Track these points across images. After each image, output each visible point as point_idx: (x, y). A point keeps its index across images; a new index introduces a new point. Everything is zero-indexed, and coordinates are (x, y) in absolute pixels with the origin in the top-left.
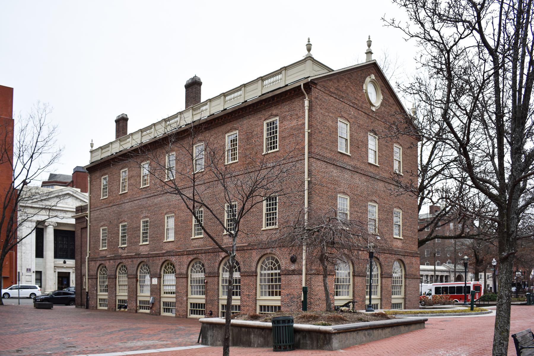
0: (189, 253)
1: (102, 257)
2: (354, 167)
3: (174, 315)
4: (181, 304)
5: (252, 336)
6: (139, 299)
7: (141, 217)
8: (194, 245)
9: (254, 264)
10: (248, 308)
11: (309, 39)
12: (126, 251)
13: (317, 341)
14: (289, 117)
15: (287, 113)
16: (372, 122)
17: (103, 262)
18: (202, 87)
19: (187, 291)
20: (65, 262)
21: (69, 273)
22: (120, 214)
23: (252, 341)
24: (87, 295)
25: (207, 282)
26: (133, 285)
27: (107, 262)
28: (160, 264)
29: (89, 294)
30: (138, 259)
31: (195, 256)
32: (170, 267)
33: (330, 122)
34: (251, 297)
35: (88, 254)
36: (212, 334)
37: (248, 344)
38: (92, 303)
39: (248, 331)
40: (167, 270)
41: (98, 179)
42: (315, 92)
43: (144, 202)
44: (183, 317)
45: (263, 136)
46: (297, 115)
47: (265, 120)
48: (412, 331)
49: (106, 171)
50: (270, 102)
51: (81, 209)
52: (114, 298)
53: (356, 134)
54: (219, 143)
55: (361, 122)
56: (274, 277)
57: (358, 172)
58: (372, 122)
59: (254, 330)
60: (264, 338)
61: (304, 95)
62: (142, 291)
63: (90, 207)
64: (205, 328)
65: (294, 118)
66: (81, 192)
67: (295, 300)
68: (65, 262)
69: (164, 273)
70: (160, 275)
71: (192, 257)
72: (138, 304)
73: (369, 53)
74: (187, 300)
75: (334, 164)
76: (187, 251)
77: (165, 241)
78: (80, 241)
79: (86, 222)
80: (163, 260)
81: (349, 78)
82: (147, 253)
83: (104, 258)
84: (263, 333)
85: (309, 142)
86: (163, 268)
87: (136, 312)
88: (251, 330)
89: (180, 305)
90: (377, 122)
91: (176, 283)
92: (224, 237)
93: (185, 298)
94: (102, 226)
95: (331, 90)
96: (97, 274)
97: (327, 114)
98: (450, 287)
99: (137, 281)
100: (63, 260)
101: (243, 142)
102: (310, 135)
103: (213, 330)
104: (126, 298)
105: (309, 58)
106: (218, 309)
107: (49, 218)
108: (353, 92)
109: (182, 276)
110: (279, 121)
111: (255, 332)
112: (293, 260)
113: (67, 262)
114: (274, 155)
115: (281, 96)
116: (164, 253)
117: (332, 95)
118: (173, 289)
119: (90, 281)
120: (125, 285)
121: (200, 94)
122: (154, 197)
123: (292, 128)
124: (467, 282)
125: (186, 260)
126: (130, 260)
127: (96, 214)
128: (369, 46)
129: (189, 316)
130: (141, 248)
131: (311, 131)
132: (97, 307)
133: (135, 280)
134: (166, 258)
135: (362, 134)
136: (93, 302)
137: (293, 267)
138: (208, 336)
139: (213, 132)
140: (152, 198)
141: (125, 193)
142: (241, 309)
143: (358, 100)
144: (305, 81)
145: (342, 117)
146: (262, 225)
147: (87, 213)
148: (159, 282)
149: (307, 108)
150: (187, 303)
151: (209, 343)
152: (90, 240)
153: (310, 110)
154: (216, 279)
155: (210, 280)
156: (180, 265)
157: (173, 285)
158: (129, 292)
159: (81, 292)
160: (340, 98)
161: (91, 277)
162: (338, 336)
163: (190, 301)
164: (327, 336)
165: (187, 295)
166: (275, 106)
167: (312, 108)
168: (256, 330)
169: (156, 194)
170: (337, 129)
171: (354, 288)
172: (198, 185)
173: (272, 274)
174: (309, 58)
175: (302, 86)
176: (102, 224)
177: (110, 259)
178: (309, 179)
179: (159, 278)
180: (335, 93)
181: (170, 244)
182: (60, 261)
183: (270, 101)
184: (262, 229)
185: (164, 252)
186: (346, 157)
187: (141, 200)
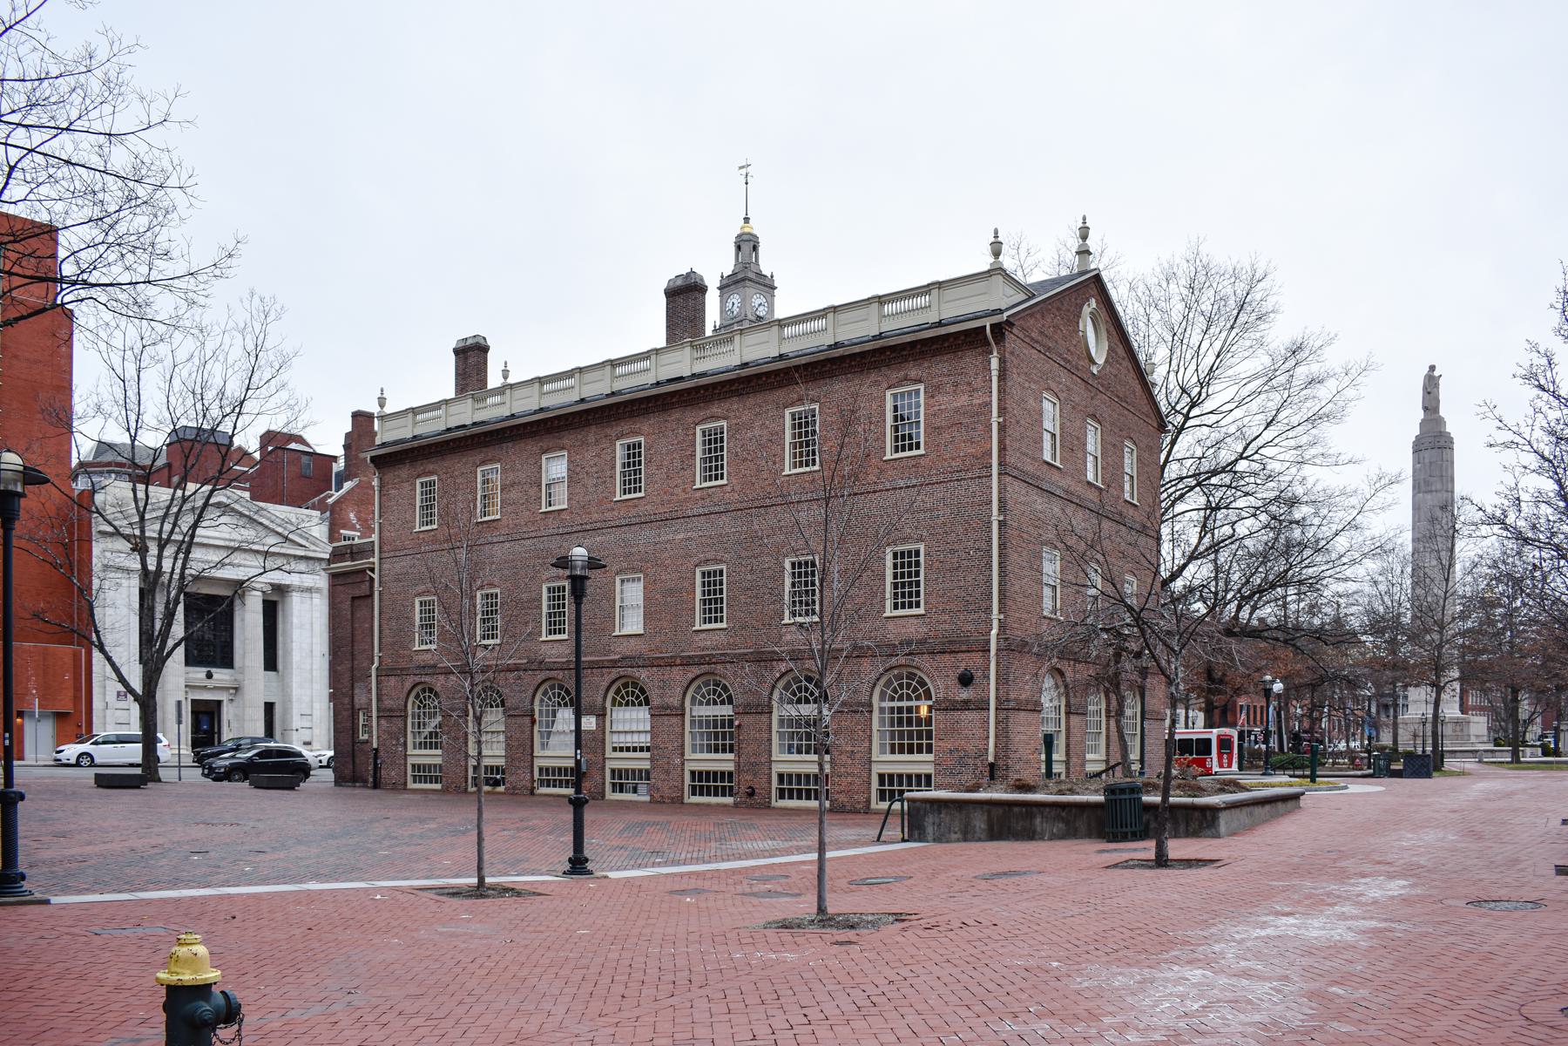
0: (687, 662)
1: (419, 667)
2: (1066, 492)
3: (647, 798)
4: (668, 772)
5: (1038, 821)
6: (538, 763)
7: (544, 577)
8: (701, 644)
9: (865, 687)
10: (849, 779)
11: (996, 232)
13: (1187, 823)
14: (949, 388)
15: (946, 379)
16: (1092, 398)
17: (427, 679)
19: (683, 746)
20: (209, 676)
21: (219, 703)
22: (475, 570)
23: (1039, 829)
24: (376, 758)
25: (739, 726)
26: (522, 732)
27: (441, 678)
28: (605, 684)
29: (381, 753)
30: (538, 672)
31: (706, 668)
32: (633, 694)
33: (1031, 401)
34: (858, 756)
35: (376, 659)
36: (937, 821)
37: (1030, 835)
38: (389, 774)
39: (1026, 811)
40: (624, 699)
41: (406, 485)
42: (1011, 341)
44: (673, 803)
45: (884, 421)
46: (969, 384)
47: (889, 388)
48: (1282, 815)
49: (431, 467)
50: (905, 353)
51: (351, 553)
52: (463, 763)
53: (1069, 424)
54: (767, 428)
55: (1077, 399)
56: (905, 715)
57: (1072, 502)
58: (1092, 398)
59: (1042, 809)
60: (1067, 823)
61: (989, 344)
62: (544, 746)
63: (380, 548)
64: (918, 810)
65: (962, 391)
66: (253, 498)
67: (971, 761)
68: (209, 676)
69: (613, 705)
70: (604, 708)
71: (696, 671)
72: (536, 776)
73: (1084, 252)
74: (683, 764)
75: (1038, 487)
76: (683, 657)
77: (617, 633)
78: (349, 627)
79: (367, 584)
80: (614, 676)
81: (1059, 309)
82: (565, 660)
83: (433, 669)
84: (1064, 814)
85: (1001, 442)
86: (611, 694)
87: (532, 793)
88: (1034, 809)
89: (663, 777)
90: (1100, 396)
91: (652, 727)
92: (784, 630)
93: (678, 761)
94: (419, 595)
95: (1033, 335)
96: (406, 706)
97: (1027, 385)
98: (1197, 740)
99: (533, 722)
100: (205, 670)
101: (833, 429)
102: (1002, 428)
103: (940, 813)
104: (501, 762)
105: (997, 271)
106: (770, 783)
107: (265, 572)
108: (1065, 338)
109: (668, 712)
110: (925, 392)
111: (1045, 814)
112: (966, 680)
113: (215, 676)
114: (913, 463)
115: (933, 344)
116: (615, 661)
117: (1035, 345)
118: (645, 740)
119: (383, 722)
120: (498, 732)
121: (704, 310)
122: (581, 534)
123: (957, 411)
124: (485, 752)
125: (679, 676)
127: (400, 565)
128: (1084, 237)
129: (686, 800)
130: (543, 647)
131: (1005, 421)
132: (405, 784)
133: (527, 720)
134: (622, 671)
135: (1078, 423)
136: (393, 773)
137: (964, 694)
138: (926, 824)
139: (751, 401)
140: (577, 535)
141: (494, 521)
142: (996, 776)
143: (1072, 354)
144: (996, 319)
145: (1049, 389)
146: (884, 607)
147: (374, 563)
148: (601, 727)
149: (995, 373)
150: (683, 770)
151: (930, 837)
152: (380, 626)
153: (1002, 376)
154: (764, 718)
155: (747, 720)
156: (660, 688)
157: (646, 732)
158: (508, 747)
159: (353, 750)
160: (1046, 351)
161: (385, 714)
162: (1227, 811)
163: (689, 767)
164: (1208, 813)
165: (683, 754)
166: (914, 360)
167: (1005, 375)
168: (1048, 810)
169: (588, 527)
170: (1041, 415)
171: (1068, 737)
172: (711, 513)
173: (900, 710)
174: (997, 271)
175: (988, 328)
176: (421, 588)
178: (1001, 518)
179: (601, 715)
180: (1037, 342)
181: (632, 641)
182: (199, 673)
183: (904, 349)
184: (885, 615)
185: (617, 657)
186: (1055, 472)
187: (541, 539)
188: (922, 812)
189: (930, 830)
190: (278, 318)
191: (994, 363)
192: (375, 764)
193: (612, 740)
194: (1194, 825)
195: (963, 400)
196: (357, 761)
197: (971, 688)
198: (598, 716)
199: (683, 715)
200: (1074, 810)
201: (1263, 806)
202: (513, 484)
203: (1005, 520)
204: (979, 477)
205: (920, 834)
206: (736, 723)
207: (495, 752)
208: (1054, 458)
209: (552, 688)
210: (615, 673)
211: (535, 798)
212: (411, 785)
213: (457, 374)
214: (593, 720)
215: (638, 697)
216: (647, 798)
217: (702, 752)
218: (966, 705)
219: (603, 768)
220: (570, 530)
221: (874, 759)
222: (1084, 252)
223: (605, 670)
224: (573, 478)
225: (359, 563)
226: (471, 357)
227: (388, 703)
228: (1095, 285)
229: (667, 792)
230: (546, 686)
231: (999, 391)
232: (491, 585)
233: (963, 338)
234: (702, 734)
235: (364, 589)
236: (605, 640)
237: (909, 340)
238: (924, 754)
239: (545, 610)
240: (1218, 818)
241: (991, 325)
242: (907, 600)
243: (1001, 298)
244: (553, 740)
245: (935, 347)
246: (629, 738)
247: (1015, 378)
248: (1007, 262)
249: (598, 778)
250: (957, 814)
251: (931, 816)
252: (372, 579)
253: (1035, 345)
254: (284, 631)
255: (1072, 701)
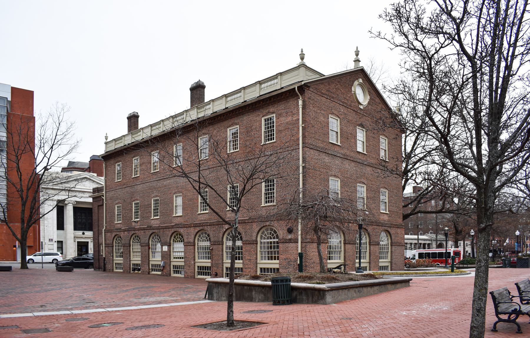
0: (195, 226)
2: (344, 155)
3: (183, 276)
4: (189, 266)
5: (254, 293)
6: (151, 263)
8: (200, 219)
9: (254, 234)
12: (139, 224)
14: (284, 114)
15: (283, 111)
16: (360, 118)
18: (206, 90)
19: (194, 257)
20: (83, 234)
21: (88, 242)
23: (254, 297)
24: (104, 260)
25: (212, 249)
26: (146, 252)
27: (122, 233)
28: (170, 234)
29: (106, 259)
31: (201, 228)
32: (179, 237)
33: (322, 118)
36: (217, 291)
37: (250, 299)
38: (108, 266)
41: (113, 166)
43: (154, 184)
44: (191, 278)
45: (261, 130)
47: (263, 116)
49: (120, 159)
52: (129, 263)
55: (350, 118)
57: (347, 159)
60: (265, 295)
61: (298, 96)
63: (106, 188)
68: (83, 234)
70: (170, 243)
71: (198, 229)
72: (151, 267)
73: (357, 61)
74: (195, 264)
75: (326, 153)
77: (174, 215)
80: (173, 231)
83: (119, 230)
84: (263, 290)
87: (149, 273)
88: (252, 288)
90: (364, 117)
93: (193, 262)
94: (117, 204)
95: (323, 91)
97: (319, 111)
99: (149, 248)
103: (218, 288)
104: (140, 262)
106: (223, 271)
109: (189, 244)
112: (290, 231)
113: (86, 234)
114: (271, 145)
115: (278, 97)
117: (324, 96)
119: (106, 248)
123: (287, 123)
125: (193, 231)
126: (142, 231)
128: (357, 55)
129: (196, 277)
132: (113, 270)
133: (147, 247)
134: (175, 229)
137: (290, 237)
139: (216, 127)
143: (347, 100)
144: (299, 84)
145: (332, 114)
149: (300, 107)
150: (195, 266)
151: (215, 299)
152: (106, 215)
154: (220, 246)
155: (215, 247)
157: (182, 252)
161: (107, 245)
163: (197, 265)
164: (321, 292)
165: (194, 260)
171: (345, 253)
173: (271, 243)
175: (296, 88)
176: (117, 202)
177: (124, 231)
178: (304, 165)
179: (169, 246)
181: (179, 218)
182: (79, 233)
183: (267, 101)
188: (212, 287)
189: (215, 295)
190: (68, 111)
191: (300, 102)
192: (104, 263)
193: (173, 255)
194: (316, 298)
195: (289, 119)
196: (100, 262)
197: (292, 233)
198: (168, 246)
199: (194, 245)
200: (267, 289)
201: (371, 287)
202: (143, 163)
203: (305, 166)
204: (295, 149)
205: (212, 297)
206: (211, 248)
207: (136, 259)
208: (337, 141)
209: (155, 236)
210: (173, 230)
211: (149, 276)
212: (115, 270)
213: (128, 126)
214: (166, 247)
215: (207, 238)
216: (183, 276)
217: (265, 259)
218: (290, 241)
219: (170, 265)
220: (159, 179)
221: (258, 262)
222: (357, 61)
223: (170, 229)
224: (161, 160)
225: (100, 194)
226: (133, 119)
227: (108, 242)
228: (361, 73)
229: (190, 274)
230: (175, 234)
231: (303, 114)
232: (137, 200)
233: (288, 93)
234: (265, 252)
235: (100, 203)
236: (170, 218)
237: (268, 97)
238: (277, 260)
239: (153, 208)
240: (326, 295)
241: (298, 87)
242: (270, 199)
243: (303, 77)
244: (156, 254)
245: (278, 98)
246: (178, 254)
247: (311, 108)
248: (307, 62)
249: (168, 268)
250: (224, 289)
251: (215, 289)
252: (103, 199)
253: (324, 96)
254: (66, 218)
255: (347, 238)
